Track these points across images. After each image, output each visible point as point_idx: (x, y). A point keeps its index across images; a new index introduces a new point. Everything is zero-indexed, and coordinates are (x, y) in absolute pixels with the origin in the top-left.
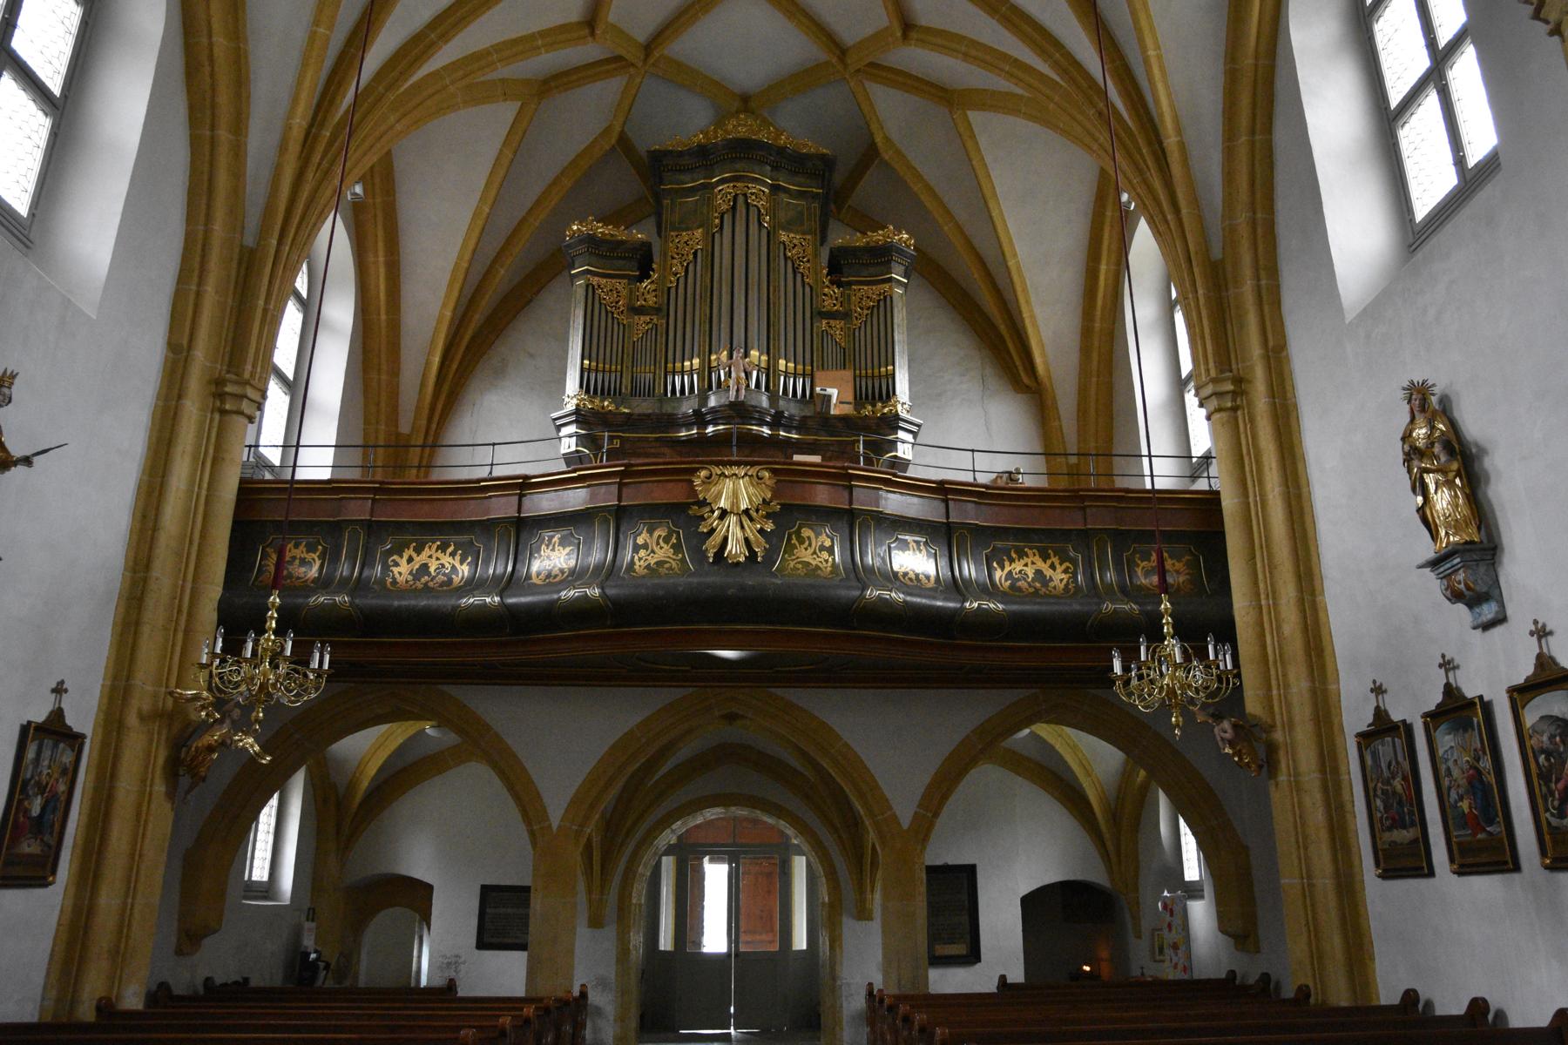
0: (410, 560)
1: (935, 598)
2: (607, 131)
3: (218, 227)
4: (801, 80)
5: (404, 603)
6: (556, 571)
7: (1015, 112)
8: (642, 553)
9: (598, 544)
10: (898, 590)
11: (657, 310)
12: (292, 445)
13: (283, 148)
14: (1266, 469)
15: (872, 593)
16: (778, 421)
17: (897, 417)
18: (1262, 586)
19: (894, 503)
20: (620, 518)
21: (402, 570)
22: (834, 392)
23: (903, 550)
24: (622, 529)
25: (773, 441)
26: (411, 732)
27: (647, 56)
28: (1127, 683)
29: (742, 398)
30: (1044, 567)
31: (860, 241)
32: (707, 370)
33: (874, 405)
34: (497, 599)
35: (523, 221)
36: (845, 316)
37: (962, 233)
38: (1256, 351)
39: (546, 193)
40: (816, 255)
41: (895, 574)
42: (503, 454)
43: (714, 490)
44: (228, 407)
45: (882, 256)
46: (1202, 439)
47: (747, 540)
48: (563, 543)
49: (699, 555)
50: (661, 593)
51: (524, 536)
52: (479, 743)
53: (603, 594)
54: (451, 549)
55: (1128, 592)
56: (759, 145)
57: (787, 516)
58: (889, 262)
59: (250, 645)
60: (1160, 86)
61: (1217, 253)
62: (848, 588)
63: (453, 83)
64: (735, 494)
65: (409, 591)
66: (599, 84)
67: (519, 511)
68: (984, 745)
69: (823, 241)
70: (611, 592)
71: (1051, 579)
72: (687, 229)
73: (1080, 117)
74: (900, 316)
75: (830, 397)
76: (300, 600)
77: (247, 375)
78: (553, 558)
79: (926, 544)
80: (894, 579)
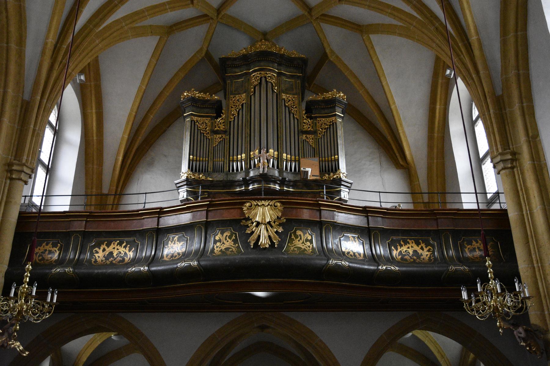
0: (104, 250)
1: (364, 264)
2: (201, 50)
3: (10, 91)
4: (290, 24)
5: (100, 271)
6: (176, 254)
7: (394, 33)
8: (218, 244)
9: (196, 240)
10: (345, 260)
11: (225, 132)
12: (47, 195)
13: (43, 53)
14: (532, 197)
15: (332, 262)
16: (283, 182)
17: (340, 180)
18: (534, 256)
19: (342, 218)
20: (207, 227)
21: (100, 255)
22: (309, 170)
23: (347, 241)
24: (208, 232)
25: (281, 193)
26: (104, 338)
27: (218, 14)
28: (470, 304)
29: (266, 172)
30: (417, 248)
31: (320, 98)
32: (249, 159)
33: (329, 174)
34: (146, 268)
35: (162, 93)
36: (314, 132)
37: (368, 93)
38: (522, 138)
39: (171, 81)
40: (299, 105)
41: (343, 253)
42: (150, 198)
43: (253, 212)
44: (14, 176)
45: (331, 104)
46: (492, 184)
47: (269, 237)
48: (179, 240)
49: (246, 244)
50: (228, 263)
51: (160, 237)
52: (139, 343)
53: (199, 264)
54: (124, 244)
55: (462, 260)
56: (271, 54)
57: (289, 225)
58: (334, 107)
59: (13, 290)
60: (467, 12)
61: (499, 93)
62: (322, 259)
63: (126, 25)
64: (264, 214)
65: (103, 265)
66: (196, 28)
67: (158, 225)
68: (389, 342)
69: (303, 99)
70: (203, 263)
71: (421, 255)
72: (239, 94)
73: (426, 31)
74: (340, 132)
75: (307, 172)
76: (47, 271)
77: (24, 161)
78: (174, 247)
79: (358, 238)
80: (343, 255)
